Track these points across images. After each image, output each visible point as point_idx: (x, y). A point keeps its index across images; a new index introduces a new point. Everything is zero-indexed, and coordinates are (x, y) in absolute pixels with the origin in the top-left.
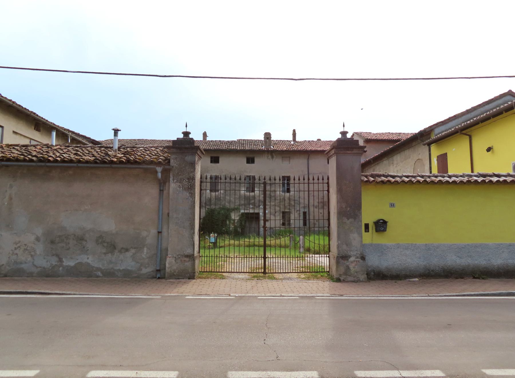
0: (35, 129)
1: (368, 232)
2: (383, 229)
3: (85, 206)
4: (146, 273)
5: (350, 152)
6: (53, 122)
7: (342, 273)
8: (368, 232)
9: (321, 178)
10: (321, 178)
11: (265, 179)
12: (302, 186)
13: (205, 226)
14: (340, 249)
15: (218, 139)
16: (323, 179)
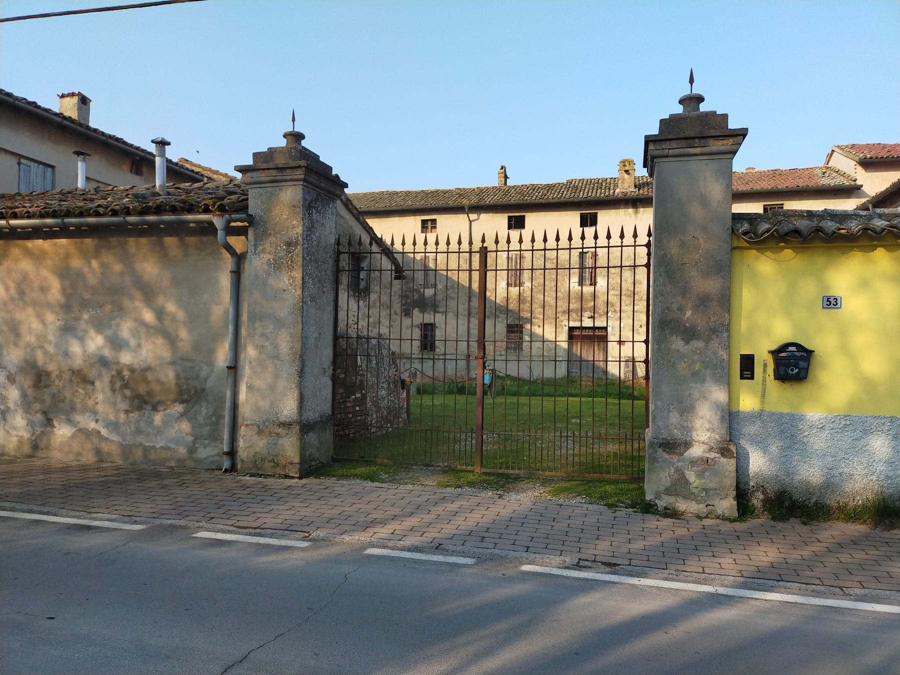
0: (133, 171)
1: (752, 378)
2: (796, 371)
3: (90, 310)
4: (206, 459)
5: (698, 150)
6: (407, 190)
7: (662, 489)
8: (752, 378)
9: (629, 234)
10: (629, 234)
11: (483, 241)
12: (564, 255)
13: (519, 329)
14: (660, 423)
15: (527, 182)
16: (635, 236)
